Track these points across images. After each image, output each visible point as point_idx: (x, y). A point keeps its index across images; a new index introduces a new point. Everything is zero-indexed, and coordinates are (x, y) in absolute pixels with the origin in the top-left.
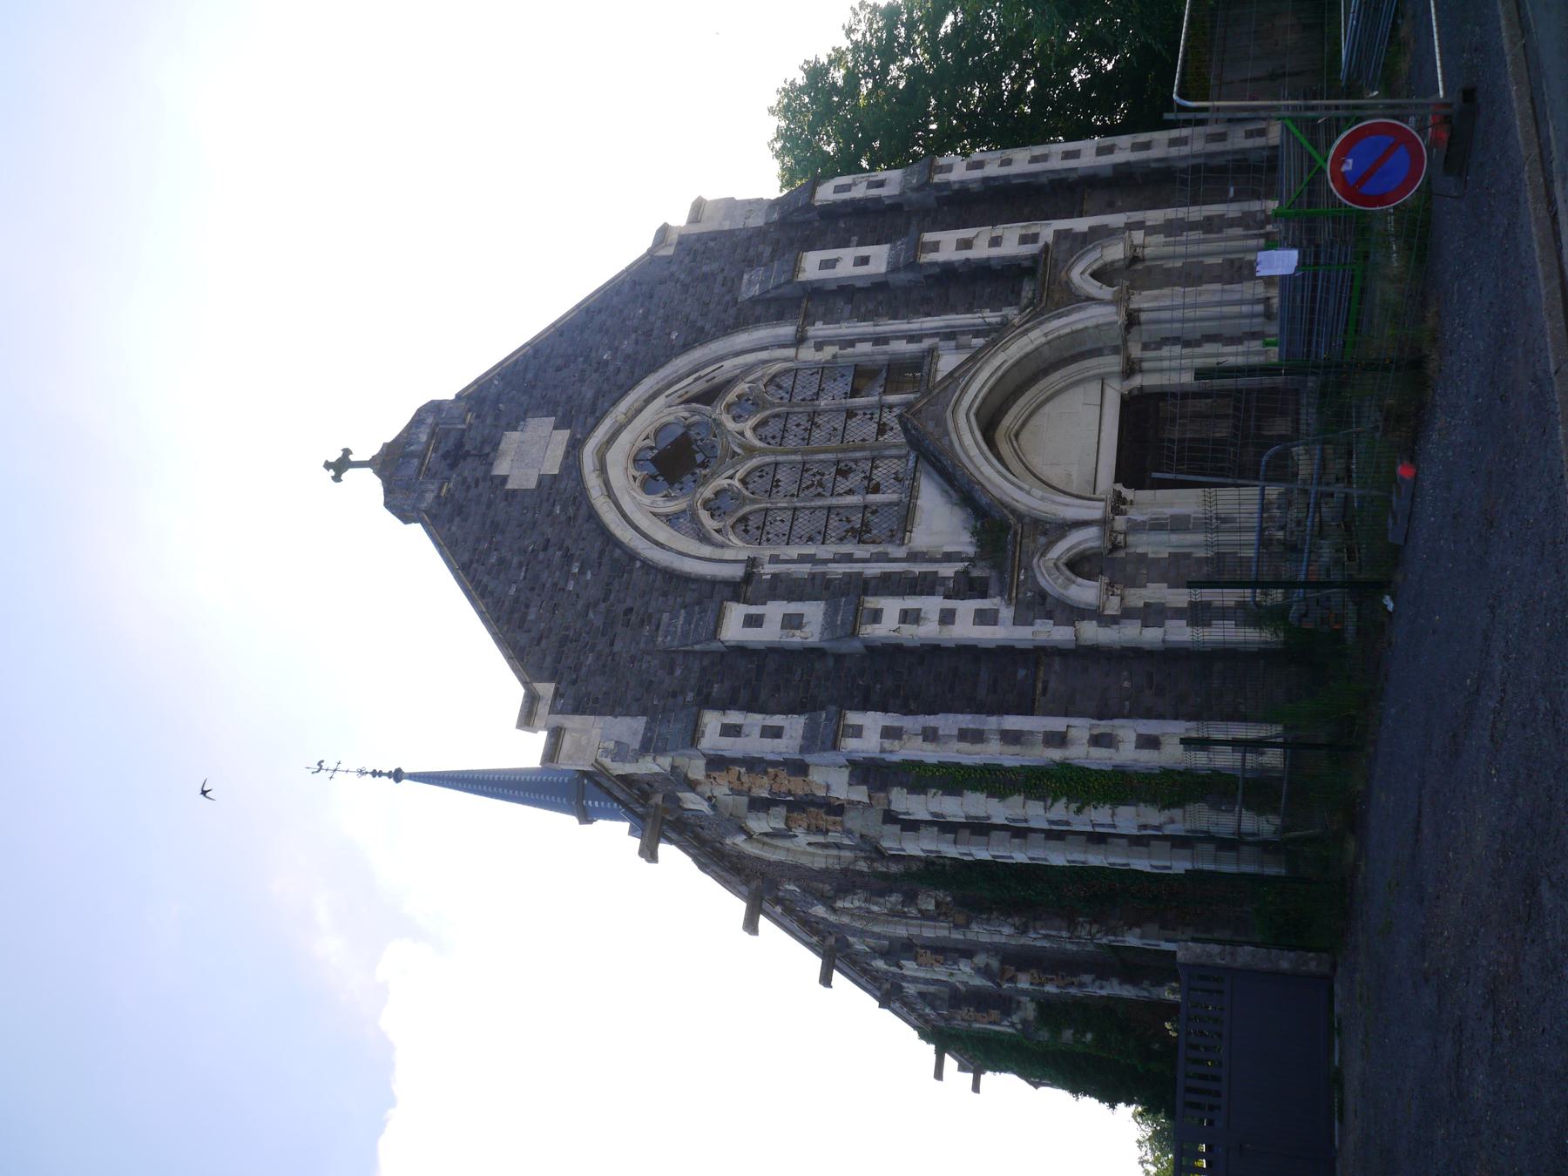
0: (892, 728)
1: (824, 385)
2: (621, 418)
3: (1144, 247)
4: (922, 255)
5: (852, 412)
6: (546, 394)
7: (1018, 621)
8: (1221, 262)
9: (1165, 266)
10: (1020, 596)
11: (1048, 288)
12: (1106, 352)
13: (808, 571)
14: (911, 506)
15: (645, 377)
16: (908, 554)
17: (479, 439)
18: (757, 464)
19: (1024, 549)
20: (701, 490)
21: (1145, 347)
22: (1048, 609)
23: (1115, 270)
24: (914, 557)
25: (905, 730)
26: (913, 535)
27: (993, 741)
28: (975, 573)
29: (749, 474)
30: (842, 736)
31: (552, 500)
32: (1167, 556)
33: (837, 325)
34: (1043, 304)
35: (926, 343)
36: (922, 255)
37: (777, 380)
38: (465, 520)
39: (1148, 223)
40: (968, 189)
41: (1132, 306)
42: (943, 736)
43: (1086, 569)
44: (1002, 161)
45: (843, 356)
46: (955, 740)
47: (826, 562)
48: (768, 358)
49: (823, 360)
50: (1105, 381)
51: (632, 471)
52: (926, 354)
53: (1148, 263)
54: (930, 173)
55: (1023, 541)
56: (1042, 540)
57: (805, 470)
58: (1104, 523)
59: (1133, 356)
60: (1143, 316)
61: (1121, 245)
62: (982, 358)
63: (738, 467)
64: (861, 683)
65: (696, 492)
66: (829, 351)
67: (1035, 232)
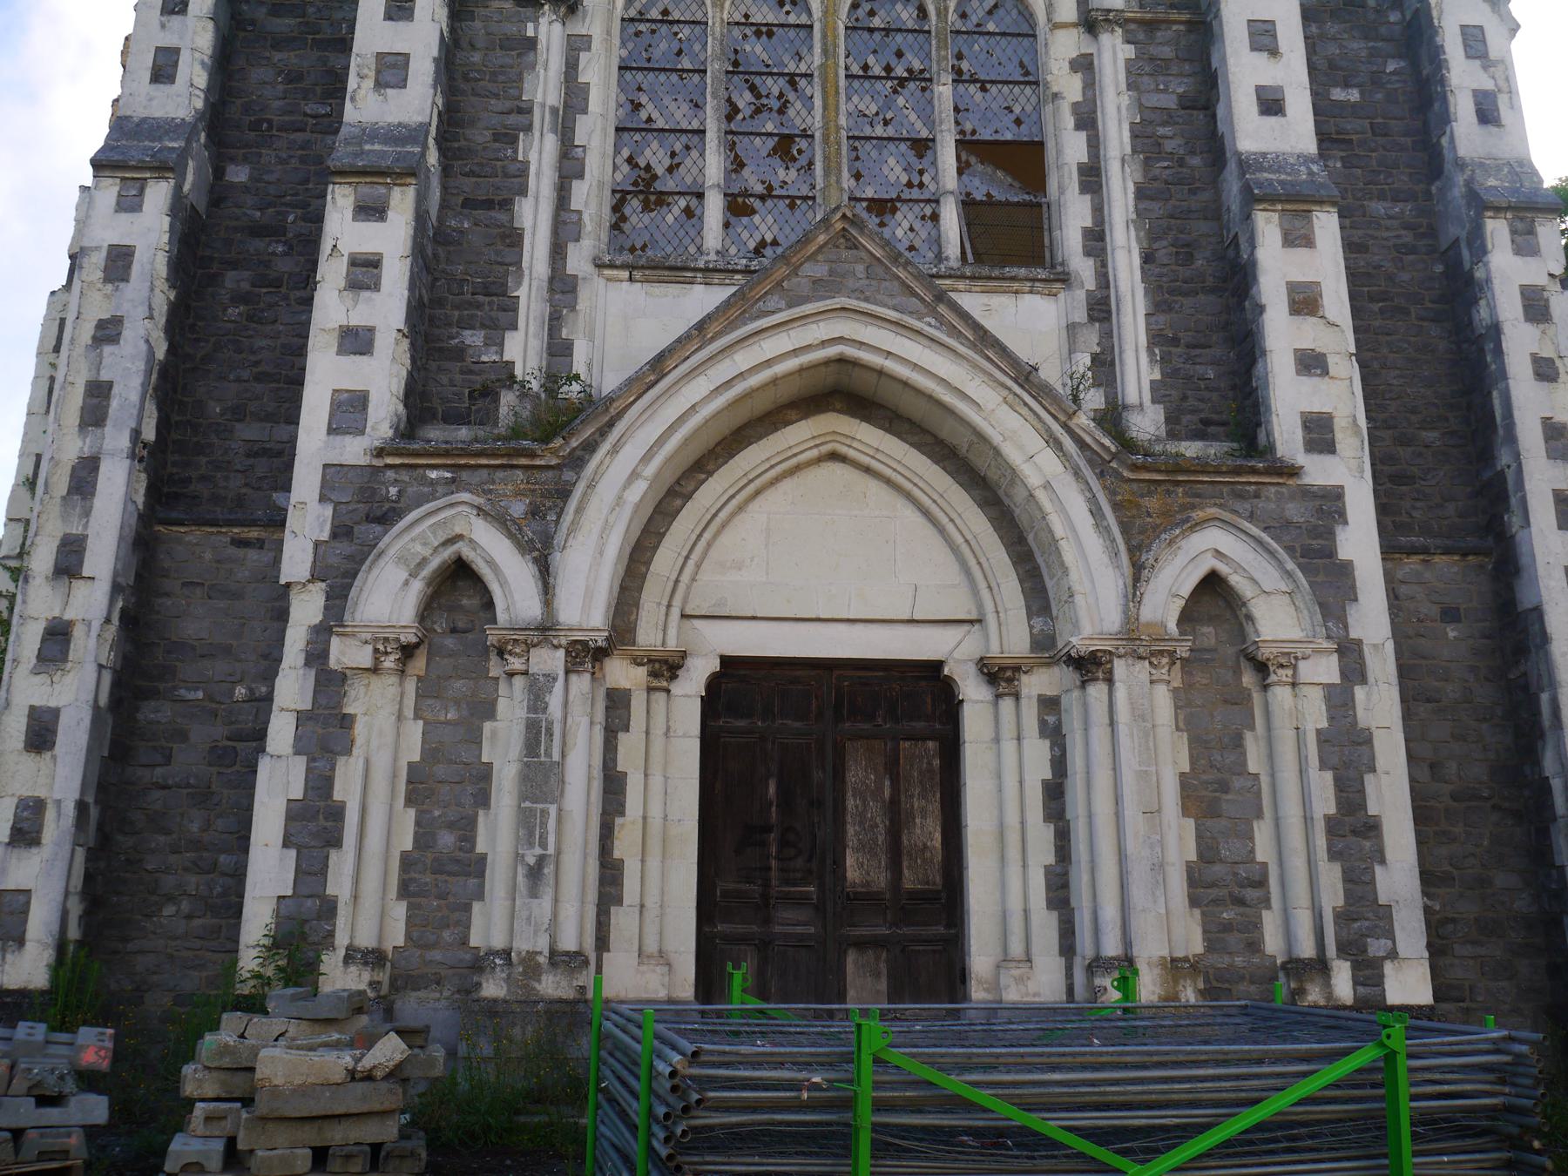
0: (128, 267)
1: (994, 88)
3: (1294, 685)
4: (1275, 216)
5: (928, 148)
7: (333, 475)
8: (1260, 857)
9: (1248, 736)
10: (390, 474)
11: (1178, 483)
12: (1038, 623)
13: (539, 98)
14: (689, 274)
16: (576, 277)
19: (500, 474)
21: (1050, 704)
22: (356, 529)
23: (1241, 624)
24: (562, 287)
25: (122, 285)
26: (626, 285)
27: (80, 444)
28: (508, 399)
30: (123, 179)
32: (485, 759)
33: (1123, 86)
34: (1126, 474)
35: (1083, 268)
36: (1275, 216)
39: (1359, 692)
40: (1476, 301)
41: (1120, 667)
42: (101, 356)
43: (465, 602)
44: (1550, 361)
45: (1056, 112)
46: (92, 377)
47: (566, 134)
49: (1049, 78)
50: (977, 626)
52: (1059, 269)
53: (1257, 697)
54: (1509, 208)
55: (519, 472)
56: (518, 509)
57: (792, 79)
58: (546, 630)
59: (1024, 678)
60: (1097, 691)
61: (1297, 634)
62: (988, 359)
64: (291, 218)
66: (1070, 87)
67: (1299, 434)
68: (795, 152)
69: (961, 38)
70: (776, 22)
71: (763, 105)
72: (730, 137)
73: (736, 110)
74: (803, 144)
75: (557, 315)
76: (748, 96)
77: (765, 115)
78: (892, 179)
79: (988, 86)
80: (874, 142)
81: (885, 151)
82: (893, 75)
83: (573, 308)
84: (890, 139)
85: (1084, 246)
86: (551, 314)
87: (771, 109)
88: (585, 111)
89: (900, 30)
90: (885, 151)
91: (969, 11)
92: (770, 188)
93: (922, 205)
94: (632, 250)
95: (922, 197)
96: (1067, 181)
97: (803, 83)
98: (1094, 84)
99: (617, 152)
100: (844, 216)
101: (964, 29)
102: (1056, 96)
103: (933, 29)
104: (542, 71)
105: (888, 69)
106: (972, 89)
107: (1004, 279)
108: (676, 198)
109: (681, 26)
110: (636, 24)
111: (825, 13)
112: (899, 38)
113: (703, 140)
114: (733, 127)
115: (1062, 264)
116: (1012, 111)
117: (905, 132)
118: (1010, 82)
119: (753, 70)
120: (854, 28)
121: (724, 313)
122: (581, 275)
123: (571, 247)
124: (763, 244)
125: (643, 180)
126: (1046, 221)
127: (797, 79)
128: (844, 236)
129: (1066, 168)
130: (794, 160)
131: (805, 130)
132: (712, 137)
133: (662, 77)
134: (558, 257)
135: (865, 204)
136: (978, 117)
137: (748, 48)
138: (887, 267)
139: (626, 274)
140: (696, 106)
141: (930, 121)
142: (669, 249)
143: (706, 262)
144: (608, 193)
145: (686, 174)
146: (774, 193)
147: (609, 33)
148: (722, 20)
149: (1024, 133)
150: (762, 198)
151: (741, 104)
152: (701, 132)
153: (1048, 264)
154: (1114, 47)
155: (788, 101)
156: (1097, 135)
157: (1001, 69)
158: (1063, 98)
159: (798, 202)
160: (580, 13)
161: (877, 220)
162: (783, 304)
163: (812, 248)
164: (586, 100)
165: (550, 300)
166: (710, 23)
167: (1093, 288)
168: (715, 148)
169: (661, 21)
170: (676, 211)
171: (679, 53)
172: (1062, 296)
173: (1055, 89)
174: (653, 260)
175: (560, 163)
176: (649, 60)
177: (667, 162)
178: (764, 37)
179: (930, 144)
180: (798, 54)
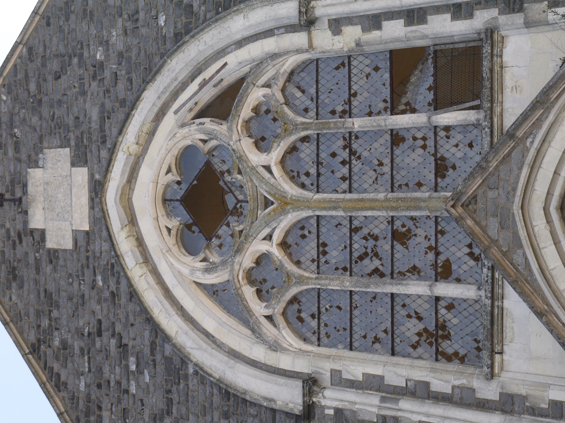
2: (134, 149)
5: (397, 133)
6: (54, 113)
13: (375, 410)
15: (144, 90)
16: (501, 394)
17: (8, 179)
18: (294, 221)
20: (238, 259)
26: (505, 357)
29: (288, 233)
31: (91, 266)
37: (296, 78)
38: (21, 287)
45: (368, 43)
48: (276, 51)
49: (346, 49)
51: (164, 221)
52: (483, 36)
57: (354, 230)
63: (274, 225)
65: (234, 262)
68: (404, 229)
69: (321, 112)
70: (316, 241)
71: (372, 251)
72: (395, 276)
73: (376, 271)
74: (398, 224)
75: (531, 410)
76: (367, 261)
77: (378, 250)
78: (420, 160)
79: (352, 92)
80: (395, 173)
81: (400, 165)
82: (348, 159)
83: (524, 398)
84: (392, 161)
85: (466, 18)
86: (530, 414)
87: (375, 246)
88: (382, 378)
89: (318, 155)
90: (400, 165)
91: (303, 107)
92: (430, 248)
93: (438, 138)
94: (479, 349)
95: (433, 138)
96: (417, 34)
97: (356, 223)
98: (348, 18)
99: (408, 356)
100: (453, 206)
101: (315, 110)
102: (358, 44)
103: (316, 132)
104: (357, 406)
105: (343, 163)
106: (355, 103)
107: (492, 78)
108: (439, 316)
109: (321, 306)
110: (321, 336)
111: (309, 208)
112: (323, 155)
113: (398, 295)
114: (388, 271)
115: (479, 34)
116: (369, 74)
117: (387, 151)
118: (350, 76)
119: (348, 257)
120: (318, 186)
121: (528, 296)
122: (499, 390)
123: (479, 395)
124: (471, 255)
125: (428, 338)
126: (447, 46)
127: (353, 227)
128: (467, 206)
129: (409, 35)
130: (409, 230)
131: (388, 222)
132: (395, 289)
133: (356, 321)
134: (487, 406)
135: (439, 180)
136: (374, 98)
137: (334, 261)
138: (489, 174)
139: (497, 357)
140: (374, 298)
141: (377, 133)
142: (477, 323)
143: (487, 297)
144: (438, 365)
145: (425, 309)
146: (434, 245)
147: (328, 357)
148: (317, 278)
149: (385, 65)
150: (437, 254)
151: (372, 267)
152: (393, 296)
153: (479, 43)
154: (324, 6)
155: (369, 234)
156: (385, 13)
157: (341, 83)
158: (360, 39)
159: (439, 228)
160: (317, 376)
161: (451, 171)
162: (520, 252)
163: (477, 230)
164: (374, 376)
165: (520, 414)
166: (319, 287)
167: (497, 10)
168: (404, 287)
169: (319, 319)
170: (449, 316)
171: (339, 308)
172: (503, 33)
173: (353, 45)
174: (487, 336)
175: (418, 398)
176: (345, 329)
177: (414, 321)
178: (326, 249)
179: (394, 132)
180: (336, 226)
